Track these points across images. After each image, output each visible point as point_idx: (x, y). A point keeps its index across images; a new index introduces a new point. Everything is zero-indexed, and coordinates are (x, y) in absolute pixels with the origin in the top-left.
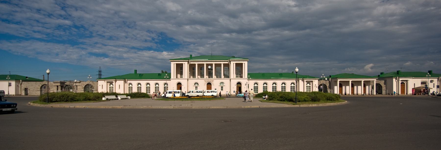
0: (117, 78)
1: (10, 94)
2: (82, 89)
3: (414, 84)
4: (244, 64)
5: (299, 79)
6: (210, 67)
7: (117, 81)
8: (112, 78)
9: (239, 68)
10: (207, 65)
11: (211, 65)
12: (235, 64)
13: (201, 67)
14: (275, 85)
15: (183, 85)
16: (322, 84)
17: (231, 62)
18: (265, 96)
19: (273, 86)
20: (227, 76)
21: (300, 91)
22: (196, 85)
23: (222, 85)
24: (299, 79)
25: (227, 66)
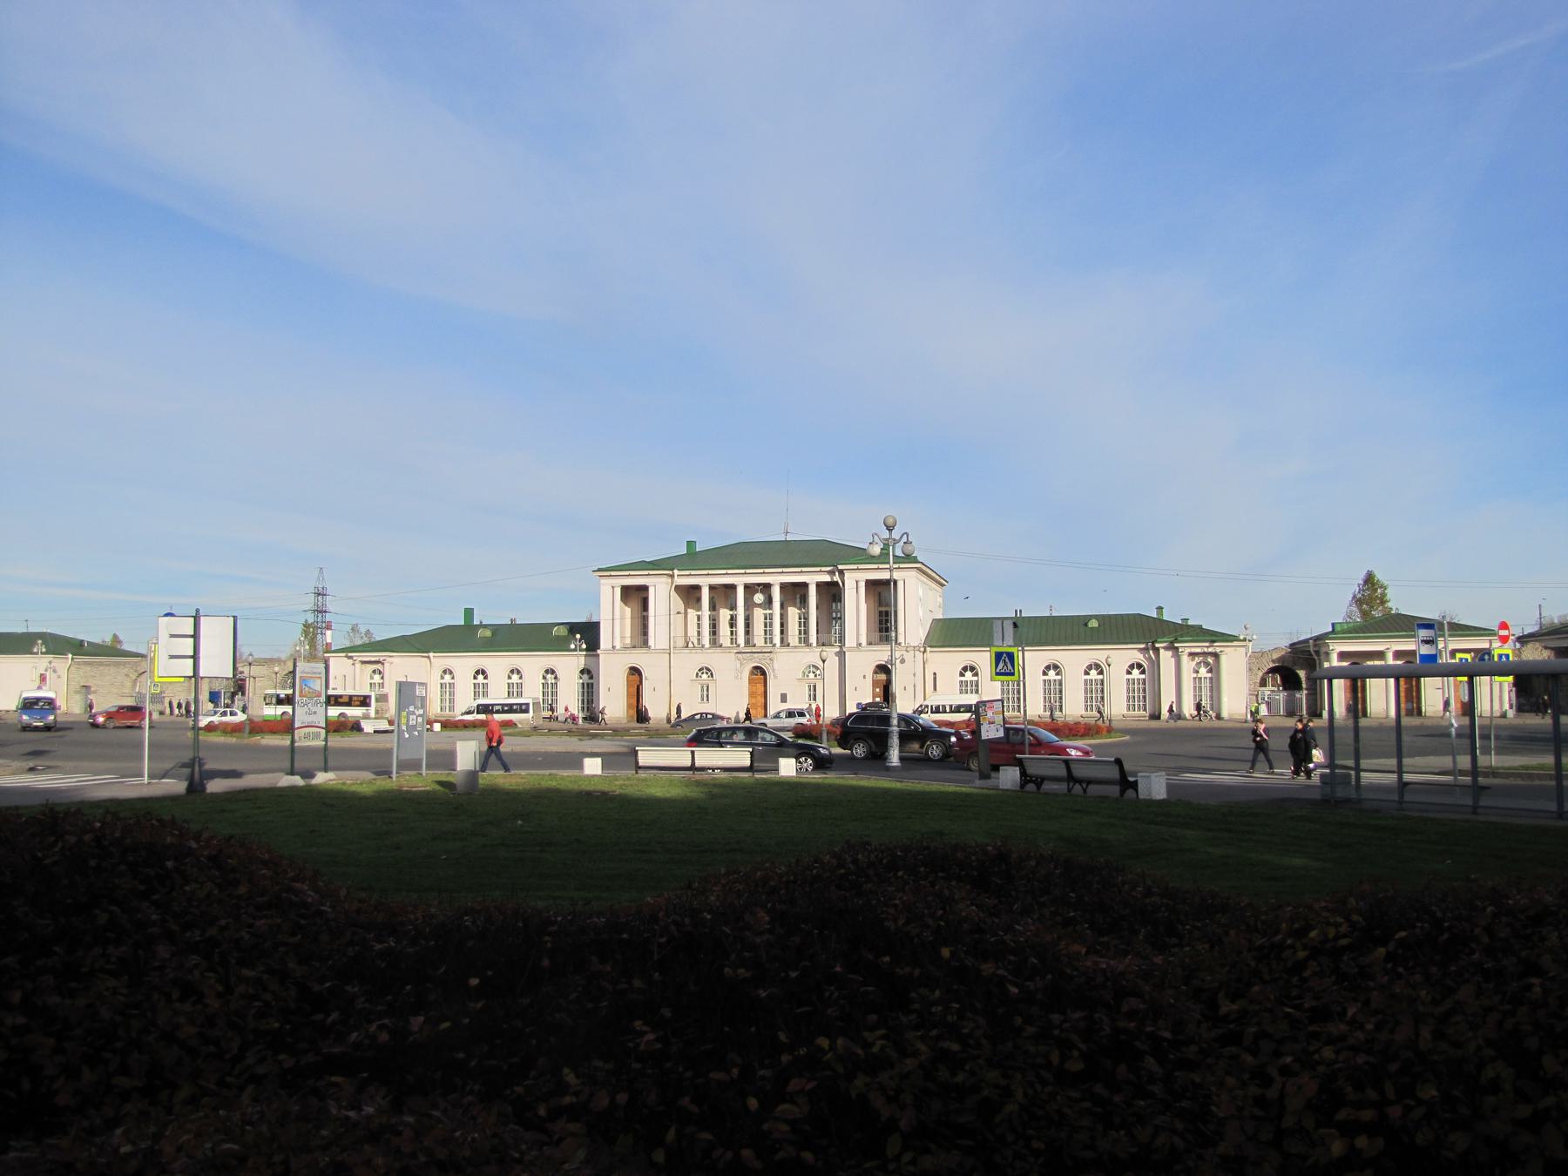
11: (766, 588)
15: (864, 677)
22: (705, 676)
25: (832, 594)
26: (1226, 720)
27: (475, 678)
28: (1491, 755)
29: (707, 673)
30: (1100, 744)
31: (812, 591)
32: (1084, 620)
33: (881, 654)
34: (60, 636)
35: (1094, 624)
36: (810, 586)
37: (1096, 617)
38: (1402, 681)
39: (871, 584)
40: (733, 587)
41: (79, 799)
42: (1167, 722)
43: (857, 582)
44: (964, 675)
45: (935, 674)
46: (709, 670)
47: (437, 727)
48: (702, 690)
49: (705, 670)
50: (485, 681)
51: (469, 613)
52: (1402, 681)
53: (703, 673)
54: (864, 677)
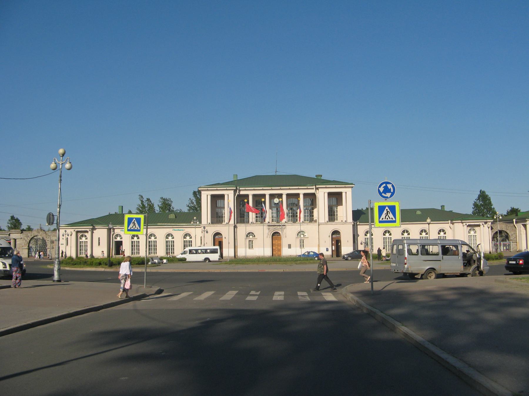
0: (93, 223)
1: (229, 256)
2: (25, 244)
3: (99, 238)
4: (344, 195)
5: (527, 219)
6: (276, 200)
7: (455, 224)
8: (84, 223)
9: (334, 200)
10: (272, 196)
11: (280, 196)
12: (209, 197)
13: (259, 200)
14: (172, 238)
15: (225, 238)
16: (497, 232)
17: (202, 192)
18: (22, 264)
19: (384, 236)
20: (310, 218)
21: (359, 249)
22: (251, 237)
23: (302, 236)
24: (527, 219)
25: (312, 199)
26: (95, 259)
27: (384, 235)
28: (372, 270)
29: (252, 235)
30: (72, 271)
31: (301, 197)
32: (415, 211)
33: (333, 227)
34: (382, 215)
35: (419, 213)
36: (300, 195)
37: (421, 210)
38: (428, 239)
39: (330, 194)
40: (298, 195)
41: (163, 293)
42: (91, 259)
43: (324, 193)
44: (168, 238)
45: (99, 238)
46: (253, 234)
47: (165, 261)
48: (301, 243)
49: (251, 234)
50: (138, 240)
51: (443, 207)
52: (428, 239)
53: (250, 235)
54: (225, 238)
